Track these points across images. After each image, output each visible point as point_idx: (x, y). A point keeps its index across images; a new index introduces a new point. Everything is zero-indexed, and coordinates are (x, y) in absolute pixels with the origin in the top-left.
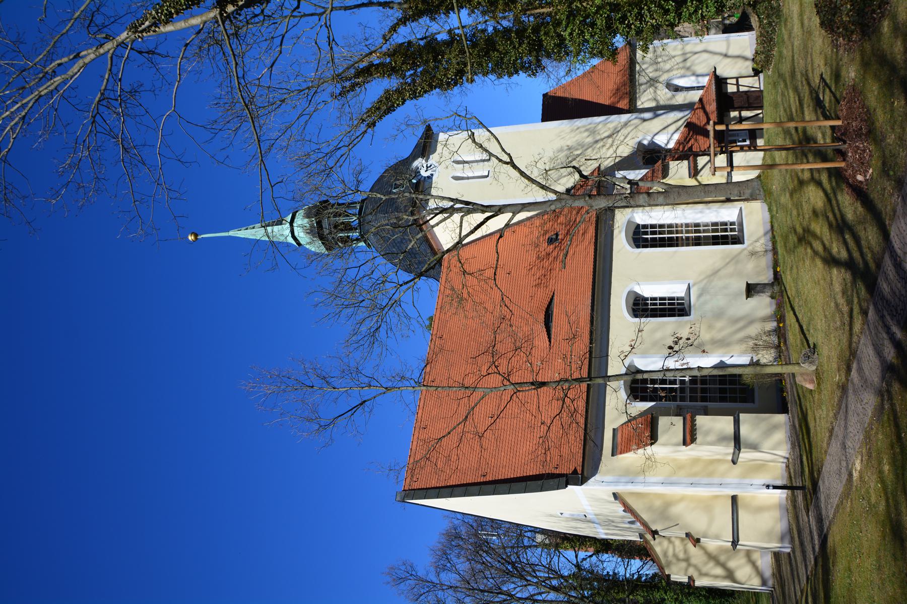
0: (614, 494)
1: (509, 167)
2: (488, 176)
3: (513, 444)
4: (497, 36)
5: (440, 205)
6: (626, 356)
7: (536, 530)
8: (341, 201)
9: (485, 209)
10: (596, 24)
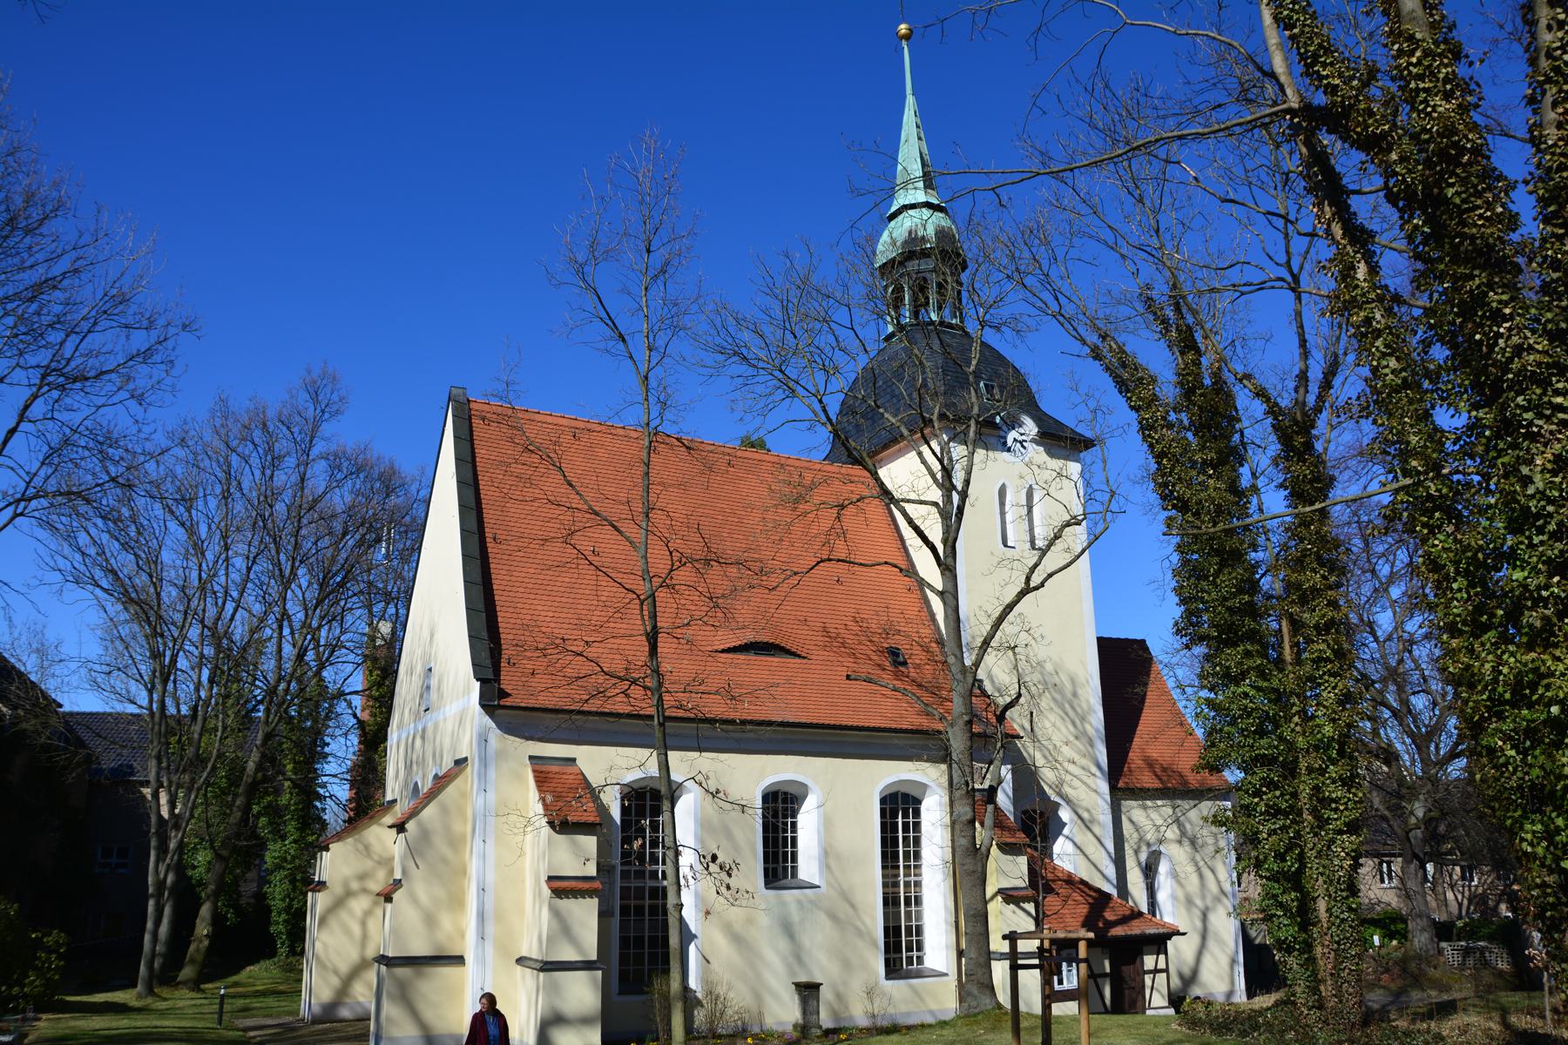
0: (466, 759)
1: (1020, 585)
2: (1006, 545)
3: (549, 588)
4: (1245, 570)
5: (957, 467)
6: (700, 784)
7: (400, 624)
8: (965, 295)
9: (950, 543)
10: (1261, 738)
